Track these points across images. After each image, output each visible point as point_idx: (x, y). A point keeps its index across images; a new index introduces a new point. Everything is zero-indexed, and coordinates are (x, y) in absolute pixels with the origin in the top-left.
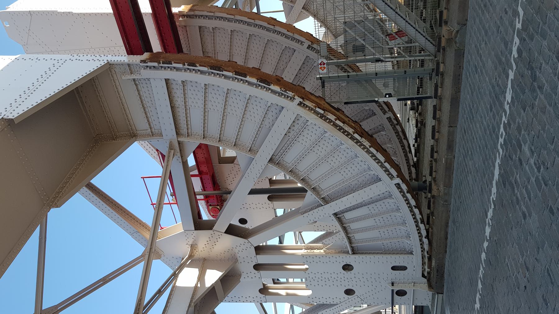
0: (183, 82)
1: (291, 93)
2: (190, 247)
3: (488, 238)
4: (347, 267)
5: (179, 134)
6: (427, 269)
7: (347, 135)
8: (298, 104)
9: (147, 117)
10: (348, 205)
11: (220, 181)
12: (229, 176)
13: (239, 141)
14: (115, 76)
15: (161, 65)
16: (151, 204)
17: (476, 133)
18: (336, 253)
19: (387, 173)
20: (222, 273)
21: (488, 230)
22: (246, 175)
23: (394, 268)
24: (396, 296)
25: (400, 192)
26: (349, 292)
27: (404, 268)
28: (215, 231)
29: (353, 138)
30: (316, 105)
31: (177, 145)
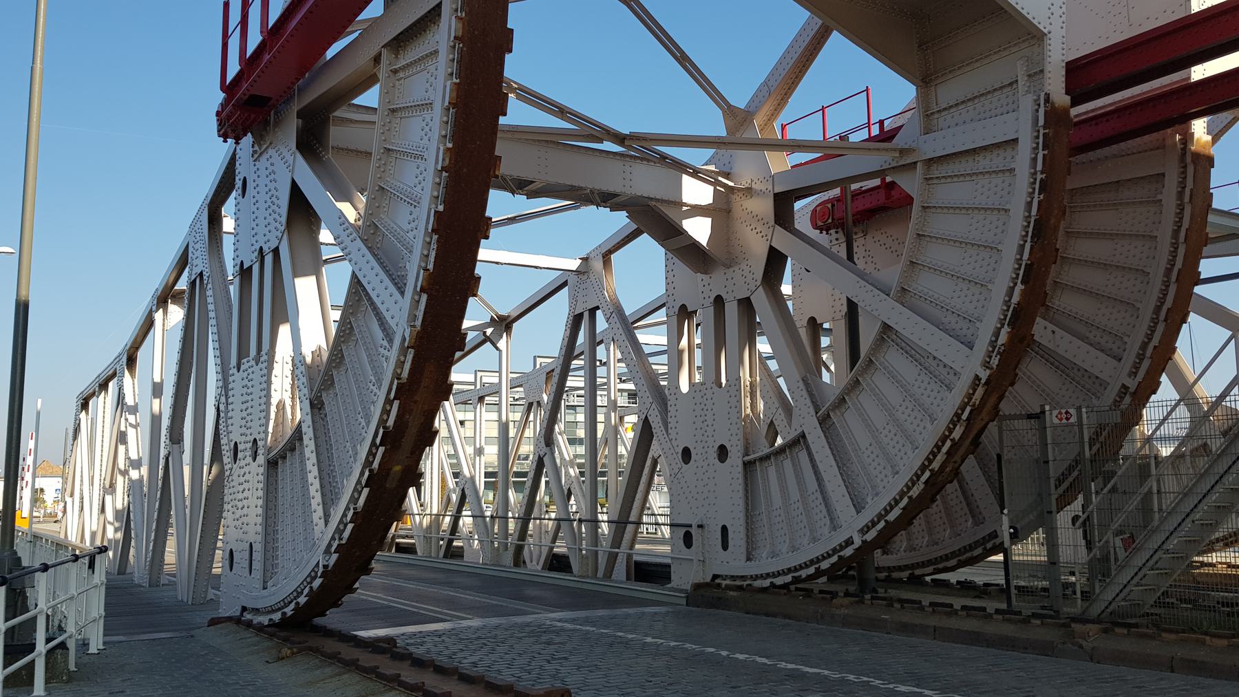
0: (1012, 170)
1: (996, 362)
2: (747, 185)
3: (731, 656)
4: (723, 452)
5: (930, 161)
6: (724, 583)
7: (927, 458)
8: (977, 376)
10: (817, 457)
11: (880, 219)
12: (888, 237)
14: (1026, 44)
15: (1042, 132)
16: (823, 106)
18: (745, 434)
19: (870, 524)
20: (705, 245)
21: (741, 657)
22: (863, 283)
23: (724, 529)
24: (682, 531)
25: (840, 545)
26: (686, 454)
27: (725, 546)
28: (774, 229)
29: (923, 468)
30: (976, 406)
31: (909, 161)
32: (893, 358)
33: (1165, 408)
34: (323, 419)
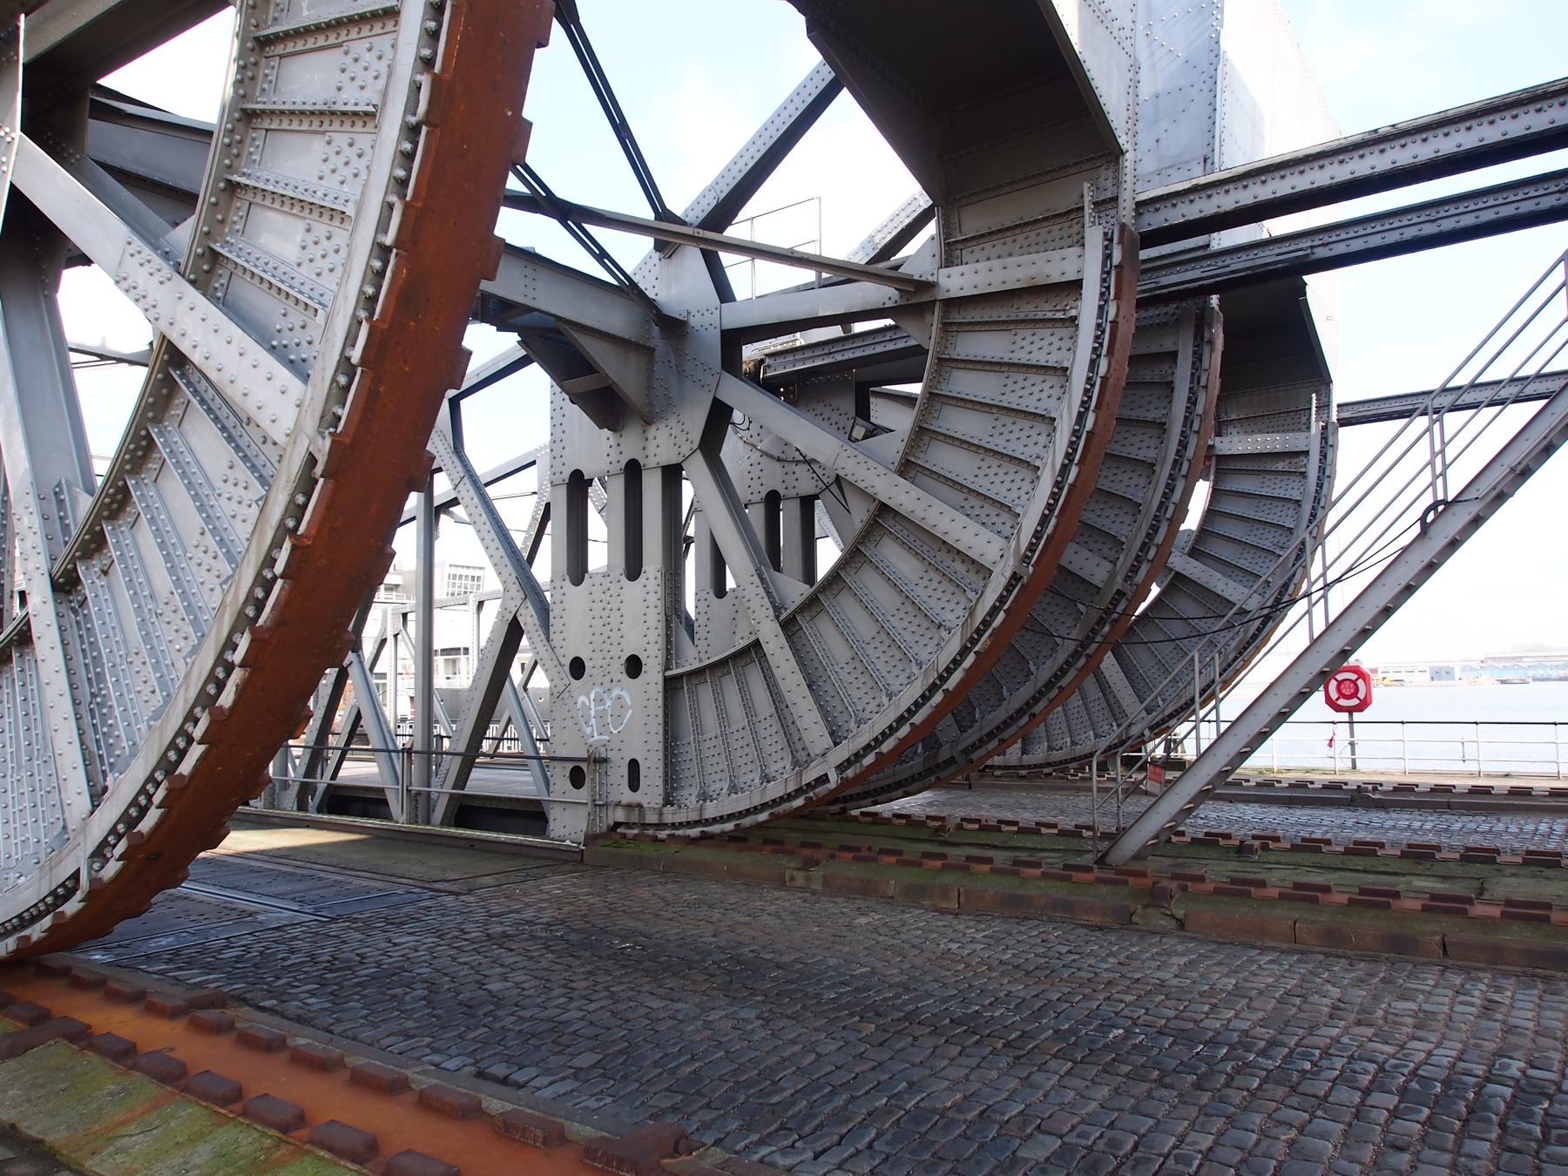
0: (1074, 319)
17: (758, 1089)
23: (634, 765)
26: (577, 668)
31: (926, 298)
32: (893, 555)
34: (75, 612)
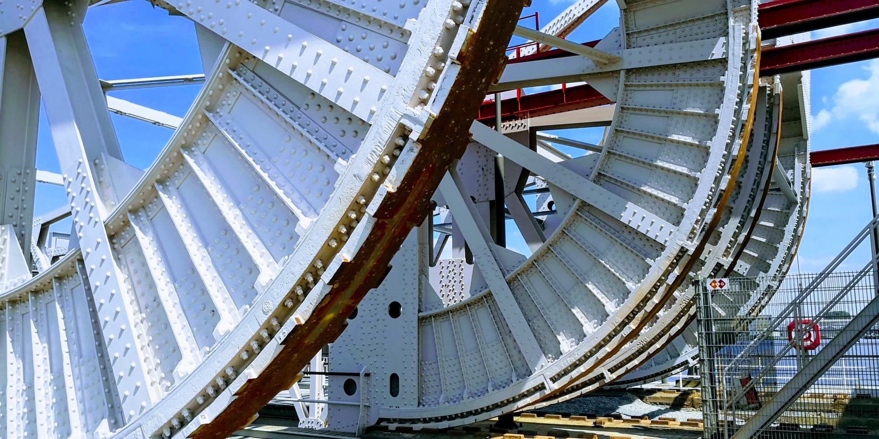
9: (658, 28)
13: (241, 93)
27: (394, 391)
33: (807, 280)
